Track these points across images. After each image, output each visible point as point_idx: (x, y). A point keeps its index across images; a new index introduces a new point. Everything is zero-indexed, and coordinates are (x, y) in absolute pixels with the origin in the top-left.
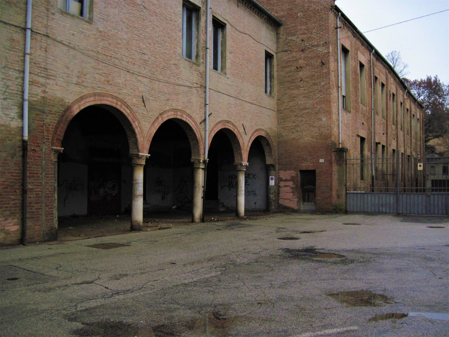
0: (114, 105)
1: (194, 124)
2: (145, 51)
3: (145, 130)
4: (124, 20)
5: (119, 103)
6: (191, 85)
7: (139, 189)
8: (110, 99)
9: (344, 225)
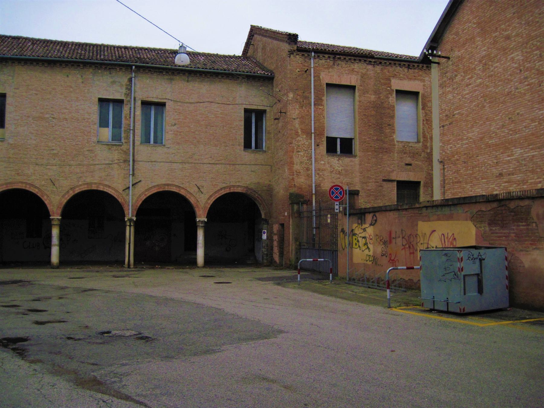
0: (24, 188)
1: (113, 191)
2: (54, 148)
3: (55, 202)
4: (33, 132)
5: (28, 186)
6: (111, 162)
7: (55, 240)
8: (20, 184)
9: (46, 309)
